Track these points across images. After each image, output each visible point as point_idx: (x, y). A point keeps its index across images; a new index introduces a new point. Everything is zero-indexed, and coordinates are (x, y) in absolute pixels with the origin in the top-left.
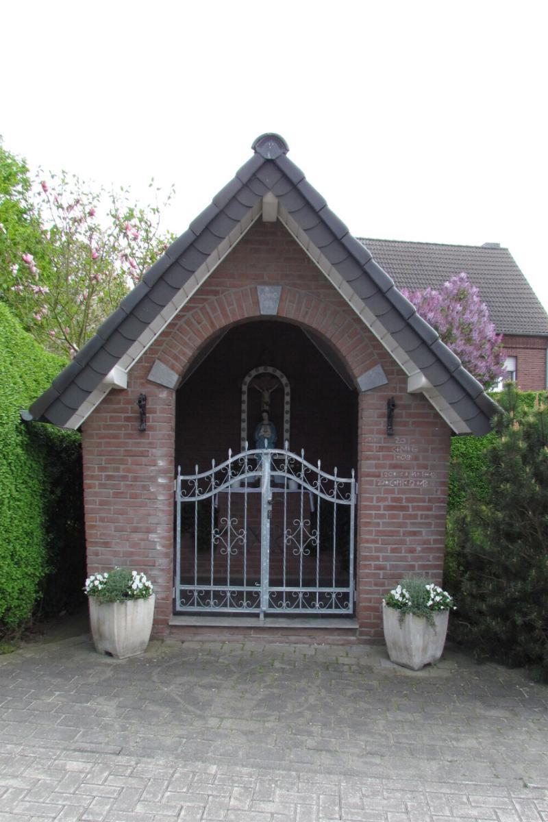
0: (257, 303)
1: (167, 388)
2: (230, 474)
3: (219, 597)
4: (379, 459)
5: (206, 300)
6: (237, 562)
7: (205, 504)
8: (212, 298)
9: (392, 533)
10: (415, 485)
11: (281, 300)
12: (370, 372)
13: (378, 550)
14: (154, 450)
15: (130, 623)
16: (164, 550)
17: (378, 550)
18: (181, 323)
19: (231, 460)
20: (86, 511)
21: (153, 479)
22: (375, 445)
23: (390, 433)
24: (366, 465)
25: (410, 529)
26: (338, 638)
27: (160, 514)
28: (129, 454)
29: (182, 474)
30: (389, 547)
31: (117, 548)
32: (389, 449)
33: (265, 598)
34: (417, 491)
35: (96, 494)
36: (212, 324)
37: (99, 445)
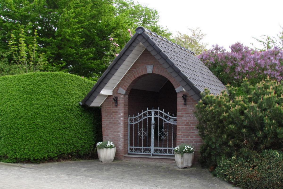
0: (146, 70)
1: (123, 94)
2: (143, 117)
3: (140, 150)
4: (182, 112)
5: (133, 70)
6: (145, 140)
7: (136, 125)
8: (135, 70)
9: (186, 132)
10: (193, 119)
11: (153, 69)
12: (179, 87)
13: (182, 137)
14: (120, 111)
15: (107, 154)
16: (122, 137)
17: (182, 137)
18: (126, 77)
19: (143, 113)
20: (102, 127)
21: (119, 118)
22: (181, 108)
23: (185, 104)
24: (178, 114)
25: (191, 131)
26: (169, 161)
27: (121, 128)
28: (113, 112)
29: (130, 117)
30: (185, 136)
31: (111, 136)
32: (185, 109)
33: (152, 150)
34: (194, 120)
35: (105, 123)
36: (135, 77)
37: (106, 110)
